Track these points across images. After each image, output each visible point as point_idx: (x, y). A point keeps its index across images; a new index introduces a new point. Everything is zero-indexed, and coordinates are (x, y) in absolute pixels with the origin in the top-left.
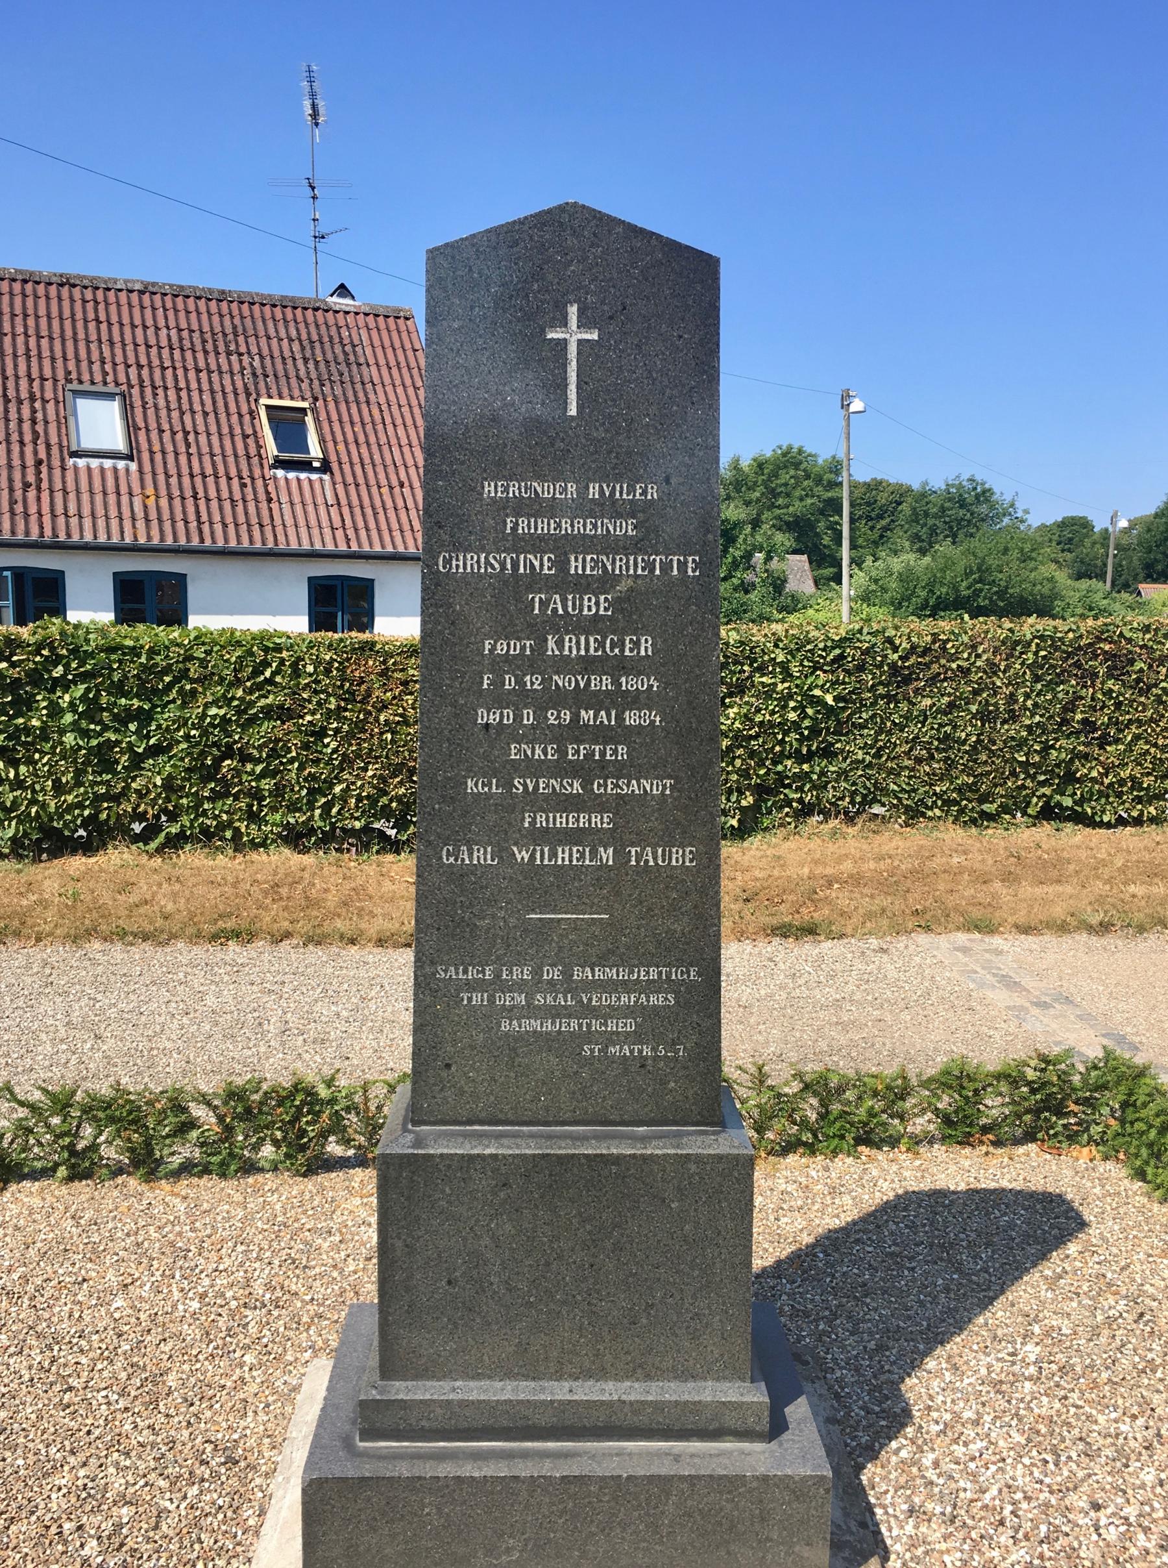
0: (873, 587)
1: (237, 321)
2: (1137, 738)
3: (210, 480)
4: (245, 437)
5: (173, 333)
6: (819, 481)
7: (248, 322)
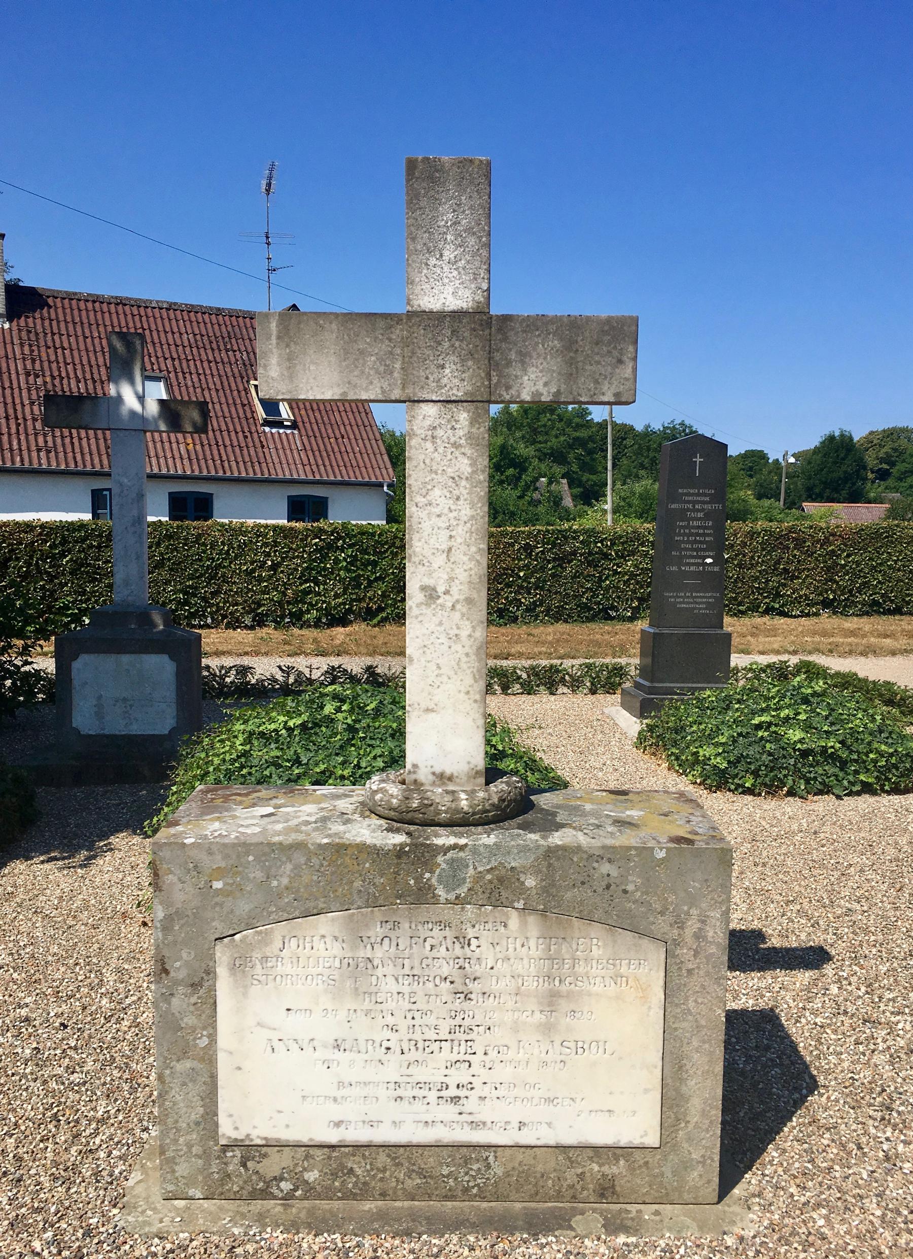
0: (622, 504)
1: (230, 328)
2: (807, 576)
3: (225, 433)
4: (243, 405)
5: (191, 336)
6: (569, 423)
7: (237, 329)
